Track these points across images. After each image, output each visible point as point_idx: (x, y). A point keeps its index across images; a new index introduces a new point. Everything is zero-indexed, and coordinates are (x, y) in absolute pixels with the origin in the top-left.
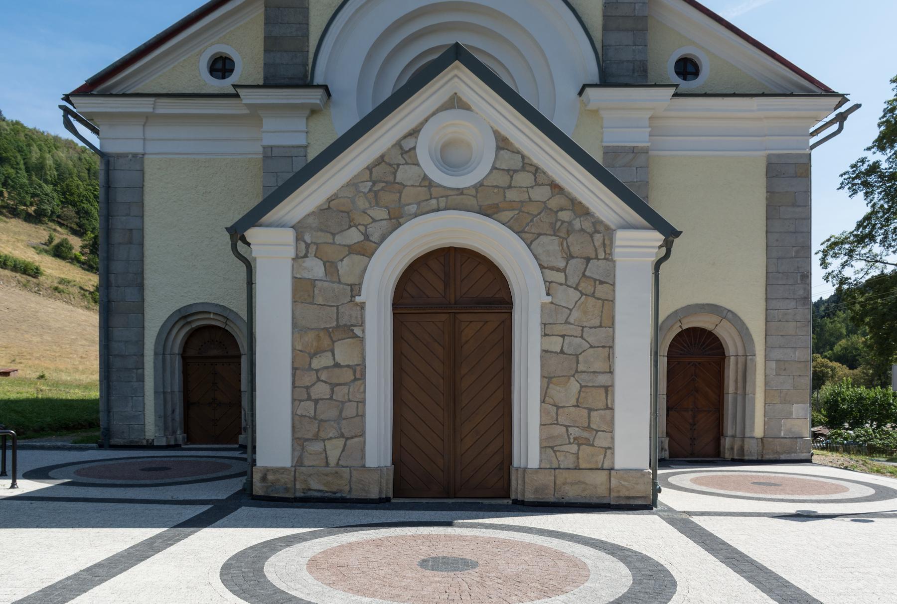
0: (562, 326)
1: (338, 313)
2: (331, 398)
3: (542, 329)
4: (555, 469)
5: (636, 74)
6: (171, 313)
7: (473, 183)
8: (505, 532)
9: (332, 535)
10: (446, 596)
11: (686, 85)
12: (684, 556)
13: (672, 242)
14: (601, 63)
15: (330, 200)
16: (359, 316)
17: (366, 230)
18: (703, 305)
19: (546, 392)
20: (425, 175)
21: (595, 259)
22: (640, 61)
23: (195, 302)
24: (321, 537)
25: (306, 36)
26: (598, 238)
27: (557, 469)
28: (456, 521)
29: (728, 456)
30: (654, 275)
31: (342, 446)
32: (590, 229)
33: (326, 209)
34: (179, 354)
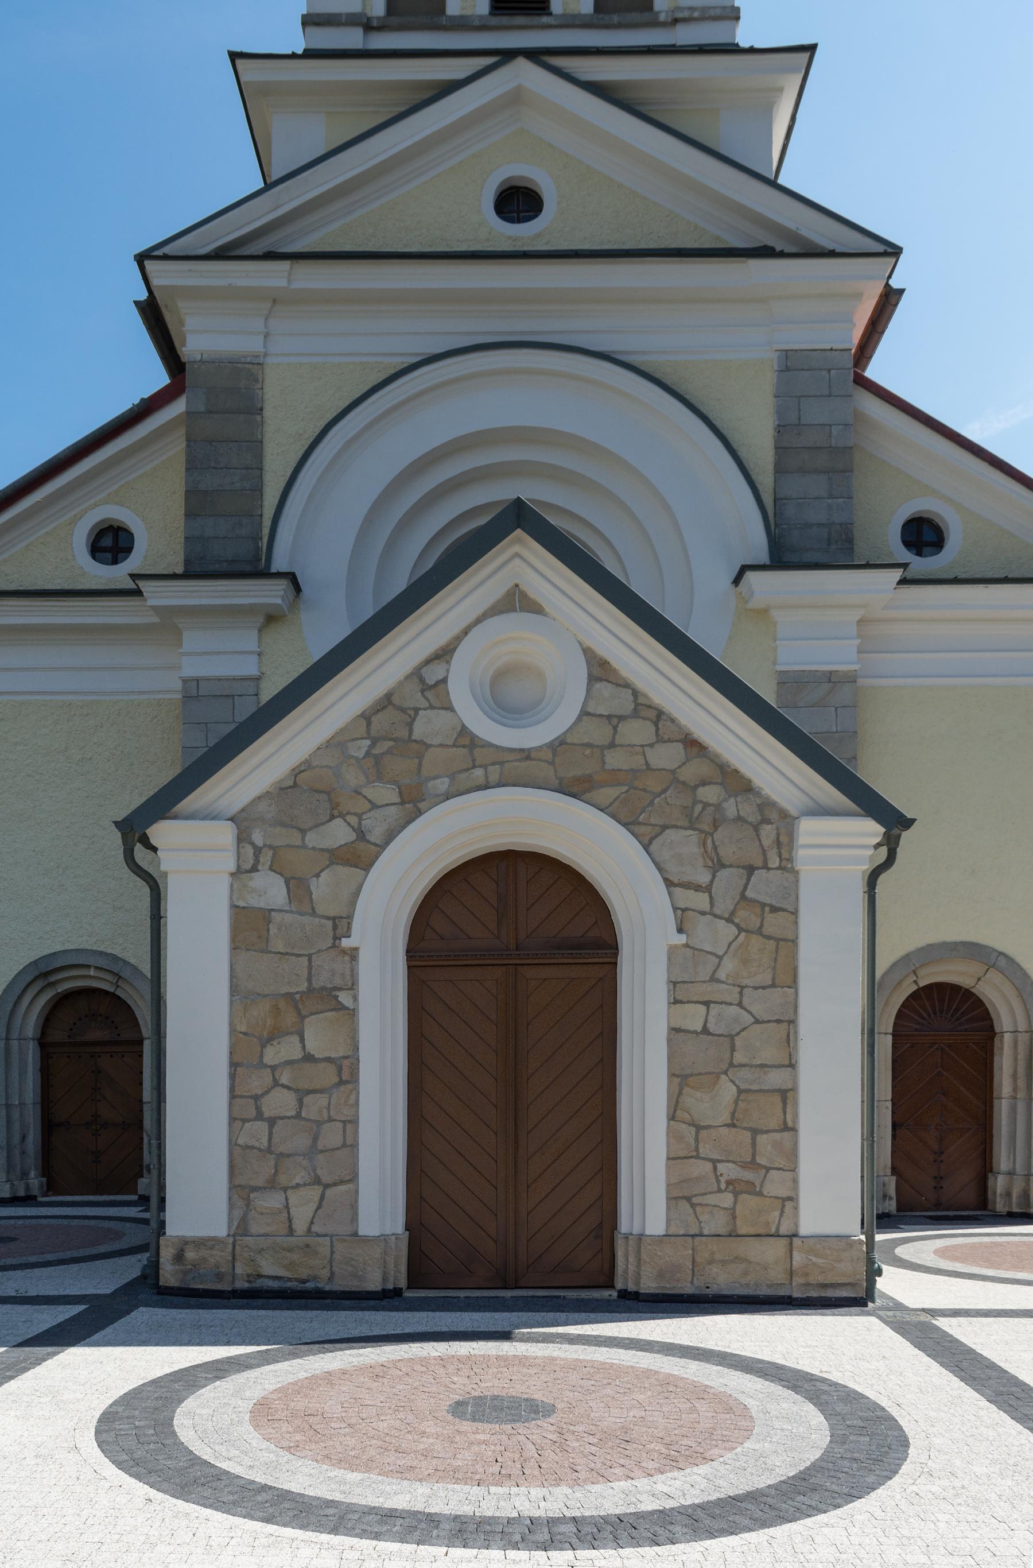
0: (705, 985)
1: (310, 967)
2: (298, 1116)
3: (669, 991)
4: (693, 1236)
5: (833, 547)
6: (21, 967)
7: (547, 740)
8: (604, 1349)
9: (298, 1357)
10: (496, 1468)
11: (920, 565)
12: (921, 1392)
13: (899, 837)
14: (773, 527)
15: (297, 772)
16: (348, 972)
17: (360, 824)
18: (955, 943)
19: (677, 1102)
20: (464, 727)
21: (762, 868)
22: (841, 524)
23: (63, 949)
24: (278, 1362)
25: (258, 490)
26: (768, 832)
27: (697, 1235)
28: (517, 1331)
29: (1000, 1207)
30: (866, 896)
31: (317, 1199)
32: (753, 818)
33: (290, 787)
34: (33, 1039)
